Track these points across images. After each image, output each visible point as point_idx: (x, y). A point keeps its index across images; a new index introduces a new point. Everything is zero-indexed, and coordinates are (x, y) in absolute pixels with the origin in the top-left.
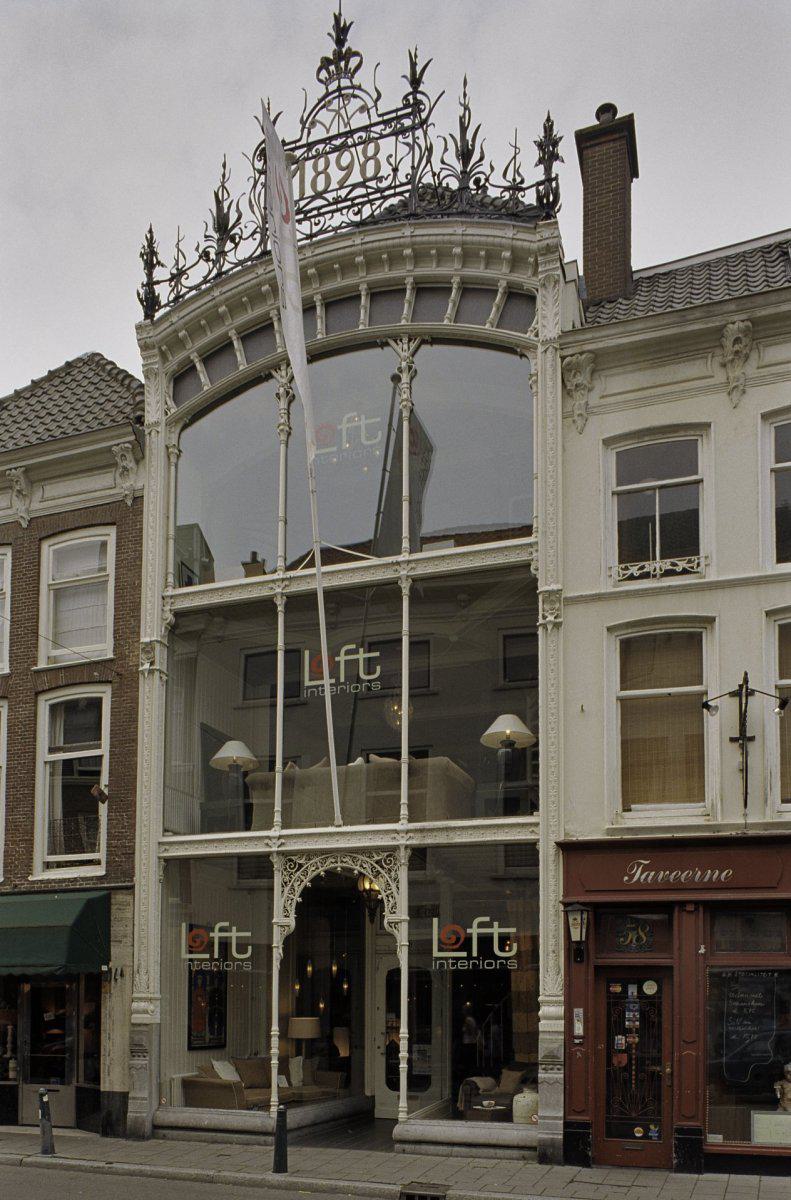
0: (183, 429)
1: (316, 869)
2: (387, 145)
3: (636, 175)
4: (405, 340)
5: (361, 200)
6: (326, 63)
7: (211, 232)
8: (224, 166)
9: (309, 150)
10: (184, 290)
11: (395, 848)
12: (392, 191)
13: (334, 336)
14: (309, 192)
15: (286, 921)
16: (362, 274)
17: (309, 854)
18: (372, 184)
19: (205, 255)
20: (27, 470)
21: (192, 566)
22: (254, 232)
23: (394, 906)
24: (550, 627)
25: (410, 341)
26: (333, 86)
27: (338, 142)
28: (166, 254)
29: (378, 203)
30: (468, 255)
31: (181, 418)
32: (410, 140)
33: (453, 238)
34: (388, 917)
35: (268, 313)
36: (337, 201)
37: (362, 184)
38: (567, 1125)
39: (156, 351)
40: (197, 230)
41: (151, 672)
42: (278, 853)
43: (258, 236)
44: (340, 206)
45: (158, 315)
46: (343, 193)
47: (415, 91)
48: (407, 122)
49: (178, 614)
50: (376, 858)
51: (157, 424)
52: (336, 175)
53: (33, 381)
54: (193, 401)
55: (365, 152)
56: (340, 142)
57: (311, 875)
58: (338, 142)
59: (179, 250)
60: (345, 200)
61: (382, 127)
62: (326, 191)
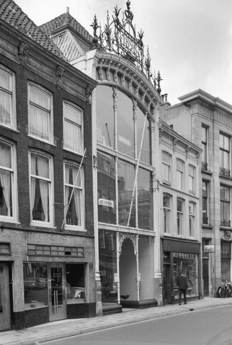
11: (136, 234)
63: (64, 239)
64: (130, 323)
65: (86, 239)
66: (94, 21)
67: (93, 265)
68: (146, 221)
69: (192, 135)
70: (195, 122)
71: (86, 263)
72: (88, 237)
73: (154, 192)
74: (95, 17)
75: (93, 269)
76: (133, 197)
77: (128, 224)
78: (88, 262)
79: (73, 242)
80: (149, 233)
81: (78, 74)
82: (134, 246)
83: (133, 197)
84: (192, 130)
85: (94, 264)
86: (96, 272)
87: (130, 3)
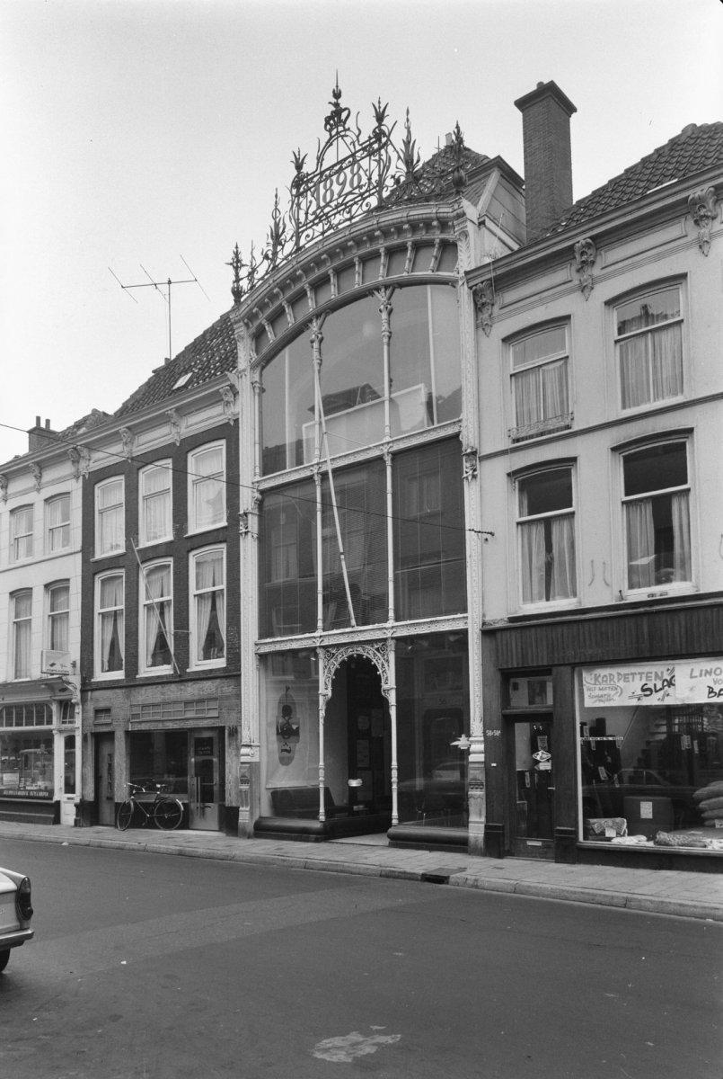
0: (263, 368)
1: (342, 656)
2: (365, 163)
3: (570, 109)
4: (383, 290)
5: (333, 212)
6: (327, 120)
7: (270, 241)
8: (276, 196)
9: (321, 177)
10: (256, 281)
11: (385, 640)
12: (368, 194)
13: (280, 335)
14: (322, 204)
15: (325, 692)
16: (354, 251)
17: (338, 646)
18: (357, 191)
19: (266, 257)
20: (177, 410)
21: (271, 459)
22: (292, 236)
23: (387, 679)
24: (470, 478)
25: (386, 290)
26: (334, 132)
27: (337, 168)
28: (245, 259)
29: (360, 203)
30: (414, 226)
31: (259, 364)
32: (377, 158)
33: (403, 219)
34: (384, 686)
35: (303, 287)
36: (337, 207)
37: (350, 193)
38: (487, 827)
39: (241, 324)
40: (263, 243)
41: (246, 533)
42: (320, 647)
43: (294, 238)
44: (339, 209)
45: (242, 300)
46: (340, 200)
47: (380, 125)
48: (376, 146)
49: (262, 492)
50: (376, 647)
51: (244, 370)
52: (336, 188)
53: (154, 372)
54: (265, 350)
55: (352, 171)
56: (339, 167)
57: (340, 660)
58: (337, 168)
60: (342, 205)
61: (362, 152)
62: (331, 201)
63: (181, 690)
64: (711, 798)
65: (224, 680)
66: (233, 255)
67: (236, 729)
72: (226, 677)
74: (237, 247)
75: (237, 739)
76: (342, 554)
77: (353, 622)
78: (227, 725)
79: (196, 692)
80: (438, 625)
83: (342, 554)
85: (239, 728)
86: (244, 745)
87: (340, 92)
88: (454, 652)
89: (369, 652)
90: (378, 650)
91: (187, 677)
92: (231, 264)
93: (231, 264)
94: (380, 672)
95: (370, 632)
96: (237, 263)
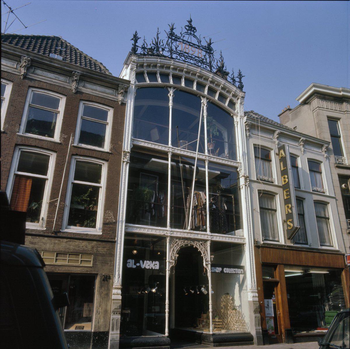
1: (181, 243)
11: (206, 241)
31: (138, 86)
59: (145, 41)
61: (182, 40)
65: (100, 243)
68: (226, 218)
69: (316, 130)
70: (318, 117)
71: (97, 274)
73: (241, 189)
74: (240, 71)
81: (112, 79)
82: (199, 250)
84: (316, 125)
88: (20, 64)
89: (196, 245)
90: (201, 244)
91: (61, 235)
92: (237, 77)
93: (237, 77)
94: (202, 255)
95: (199, 235)
96: (136, 38)
